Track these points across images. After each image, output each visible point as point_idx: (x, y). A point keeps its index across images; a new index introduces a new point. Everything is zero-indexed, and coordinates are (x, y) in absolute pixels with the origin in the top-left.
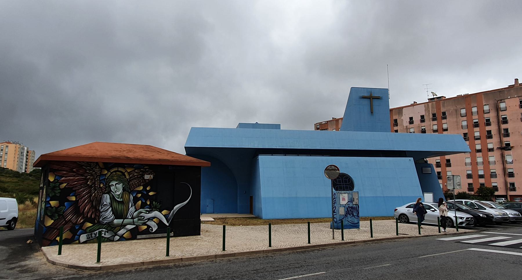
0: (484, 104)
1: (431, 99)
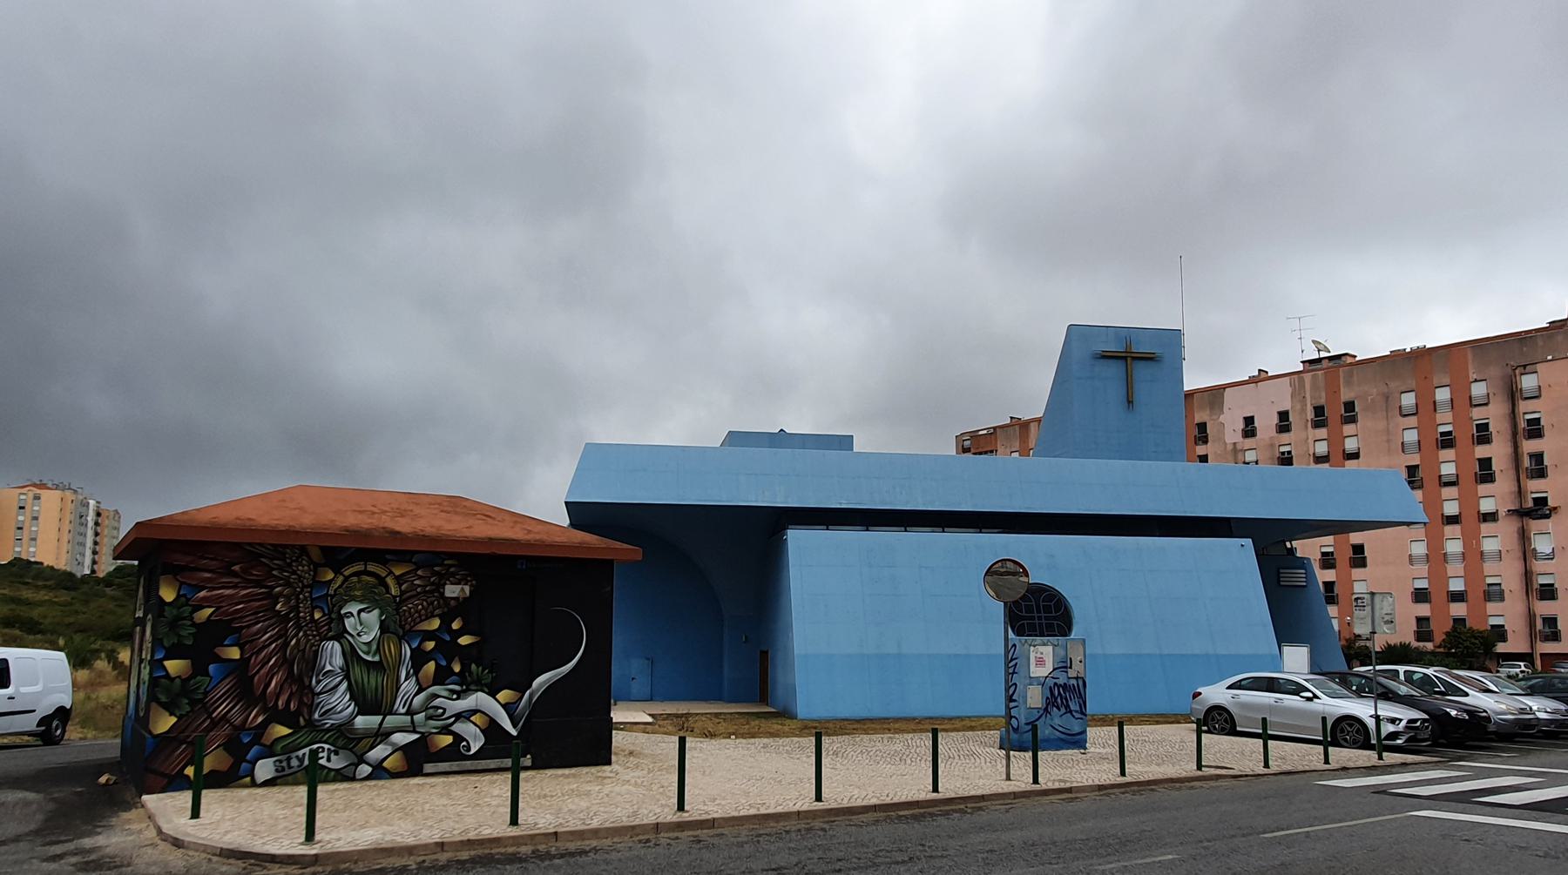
0: (1473, 376)
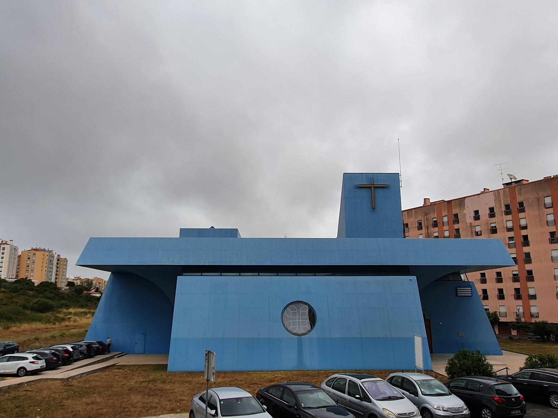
1: (507, 184)
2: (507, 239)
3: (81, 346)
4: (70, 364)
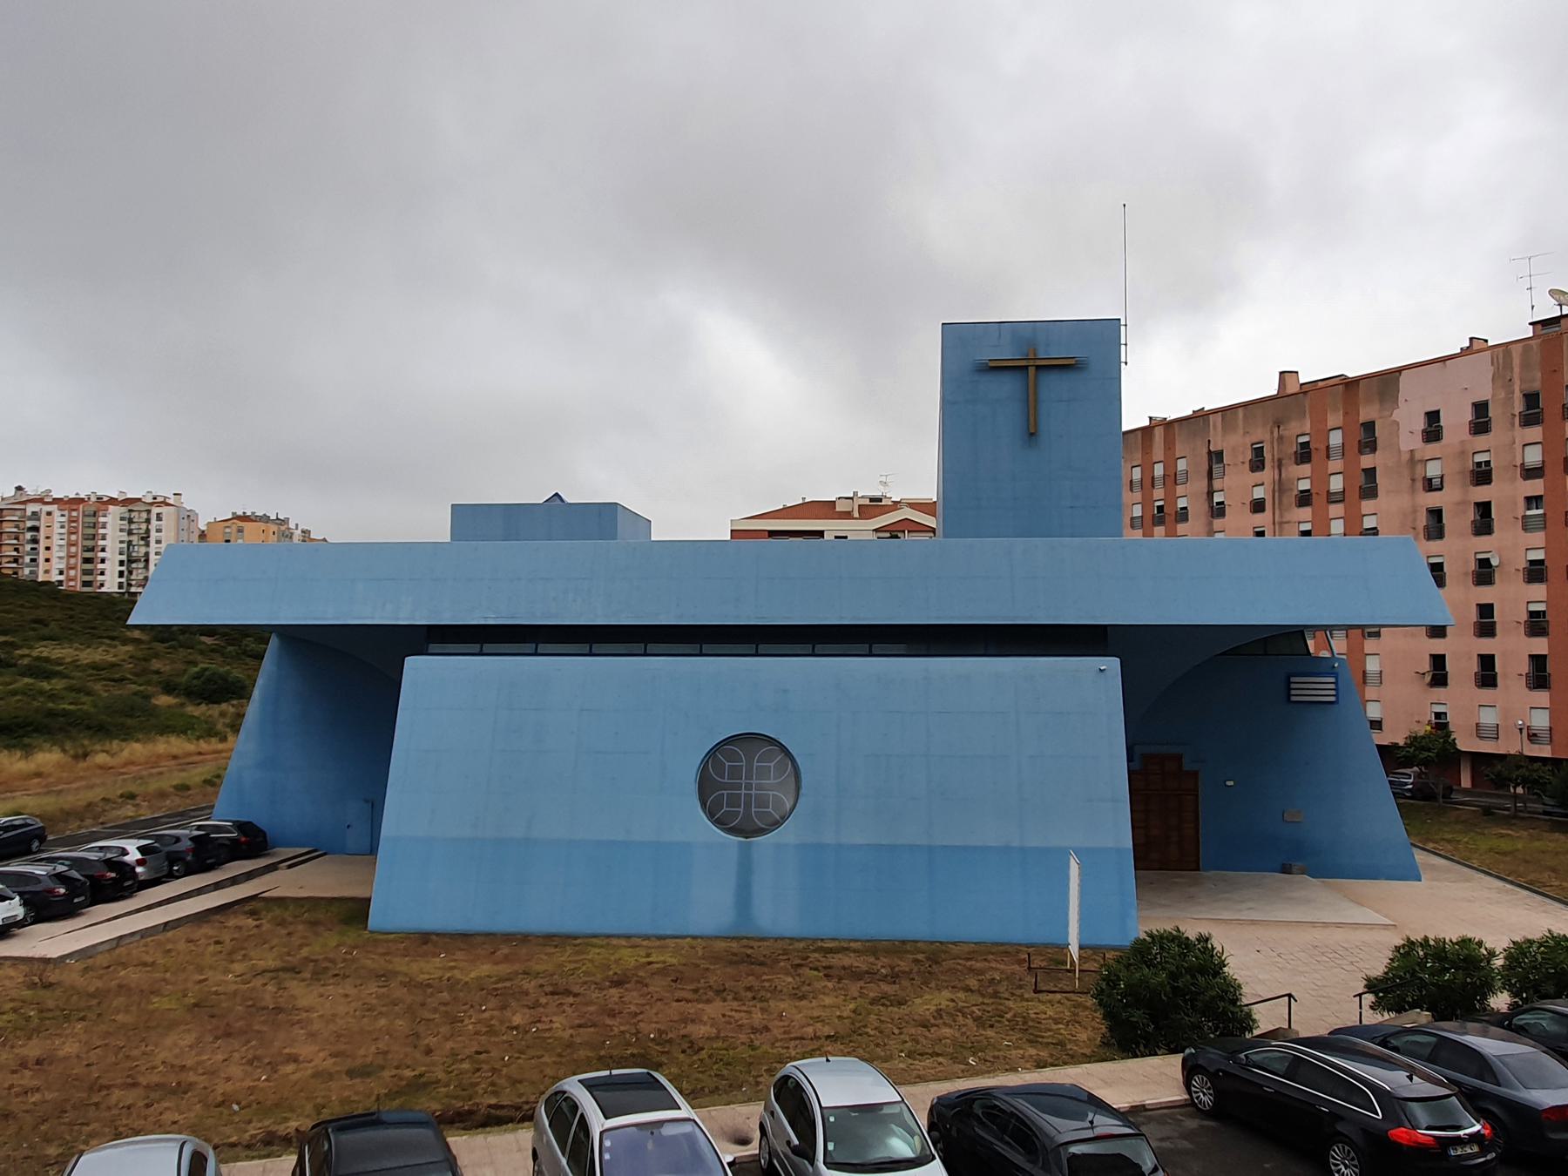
2: (1521, 503)
3: (178, 839)
4: (130, 896)
